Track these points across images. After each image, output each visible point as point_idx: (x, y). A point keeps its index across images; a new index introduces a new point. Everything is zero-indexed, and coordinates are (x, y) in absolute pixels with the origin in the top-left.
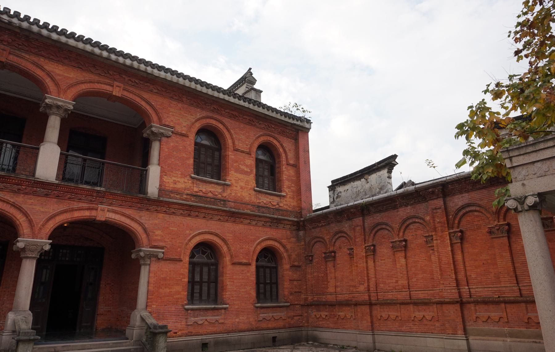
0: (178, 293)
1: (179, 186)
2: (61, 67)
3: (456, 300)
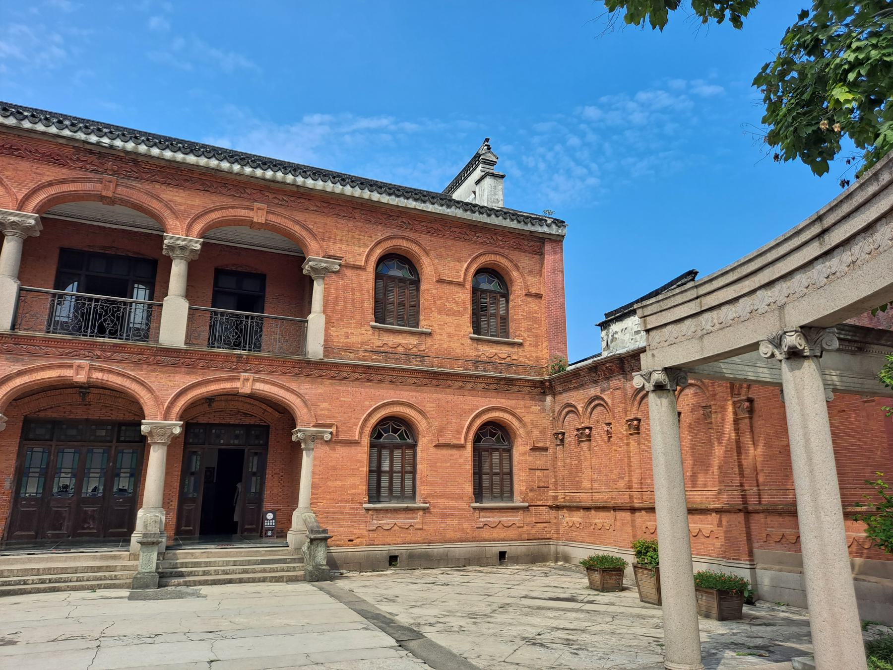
0: (354, 486)
1: (353, 339)
2: (183, 193)
3: (737, 507)
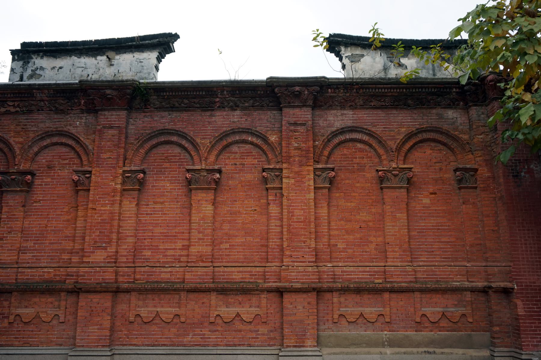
3: (314, 285)
